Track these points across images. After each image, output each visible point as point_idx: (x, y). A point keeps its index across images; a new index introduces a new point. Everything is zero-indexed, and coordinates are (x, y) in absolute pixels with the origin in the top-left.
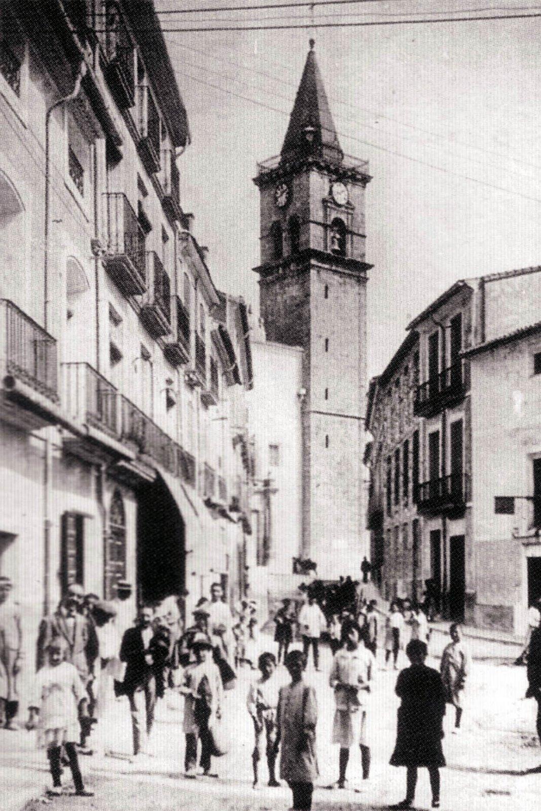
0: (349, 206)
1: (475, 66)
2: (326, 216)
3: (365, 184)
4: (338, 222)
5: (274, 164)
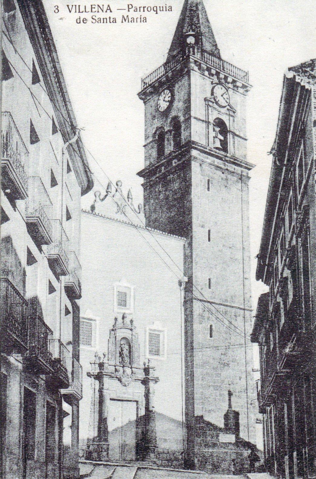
4: (220, 123)
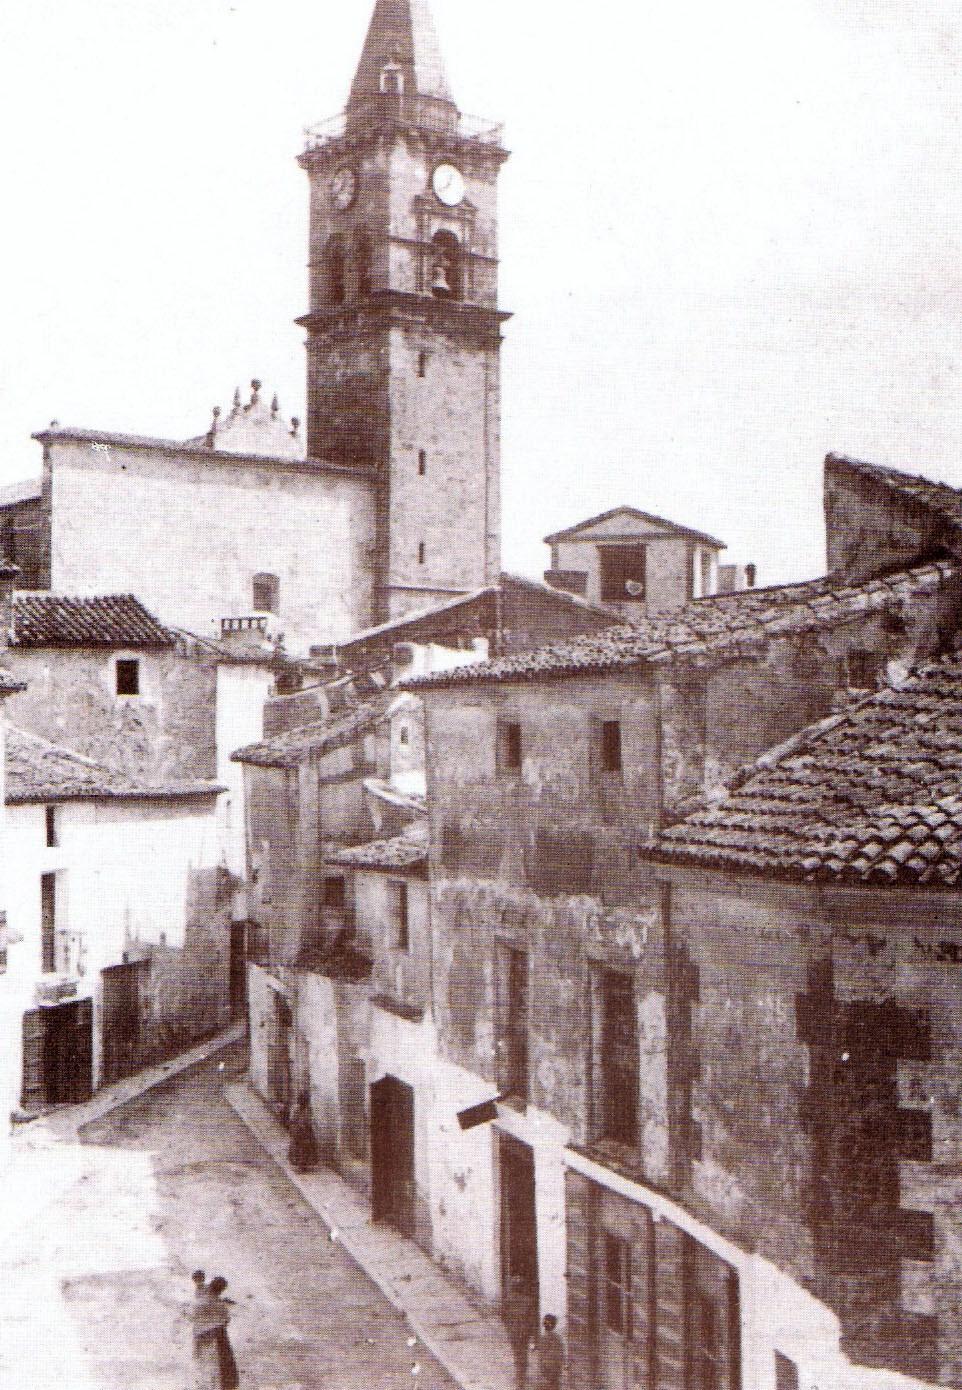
0: (466, 211)
1: (26, 622)
2: (421, 227)
3: (499, 163)
4: (444, 237)
5: (337, 127)
